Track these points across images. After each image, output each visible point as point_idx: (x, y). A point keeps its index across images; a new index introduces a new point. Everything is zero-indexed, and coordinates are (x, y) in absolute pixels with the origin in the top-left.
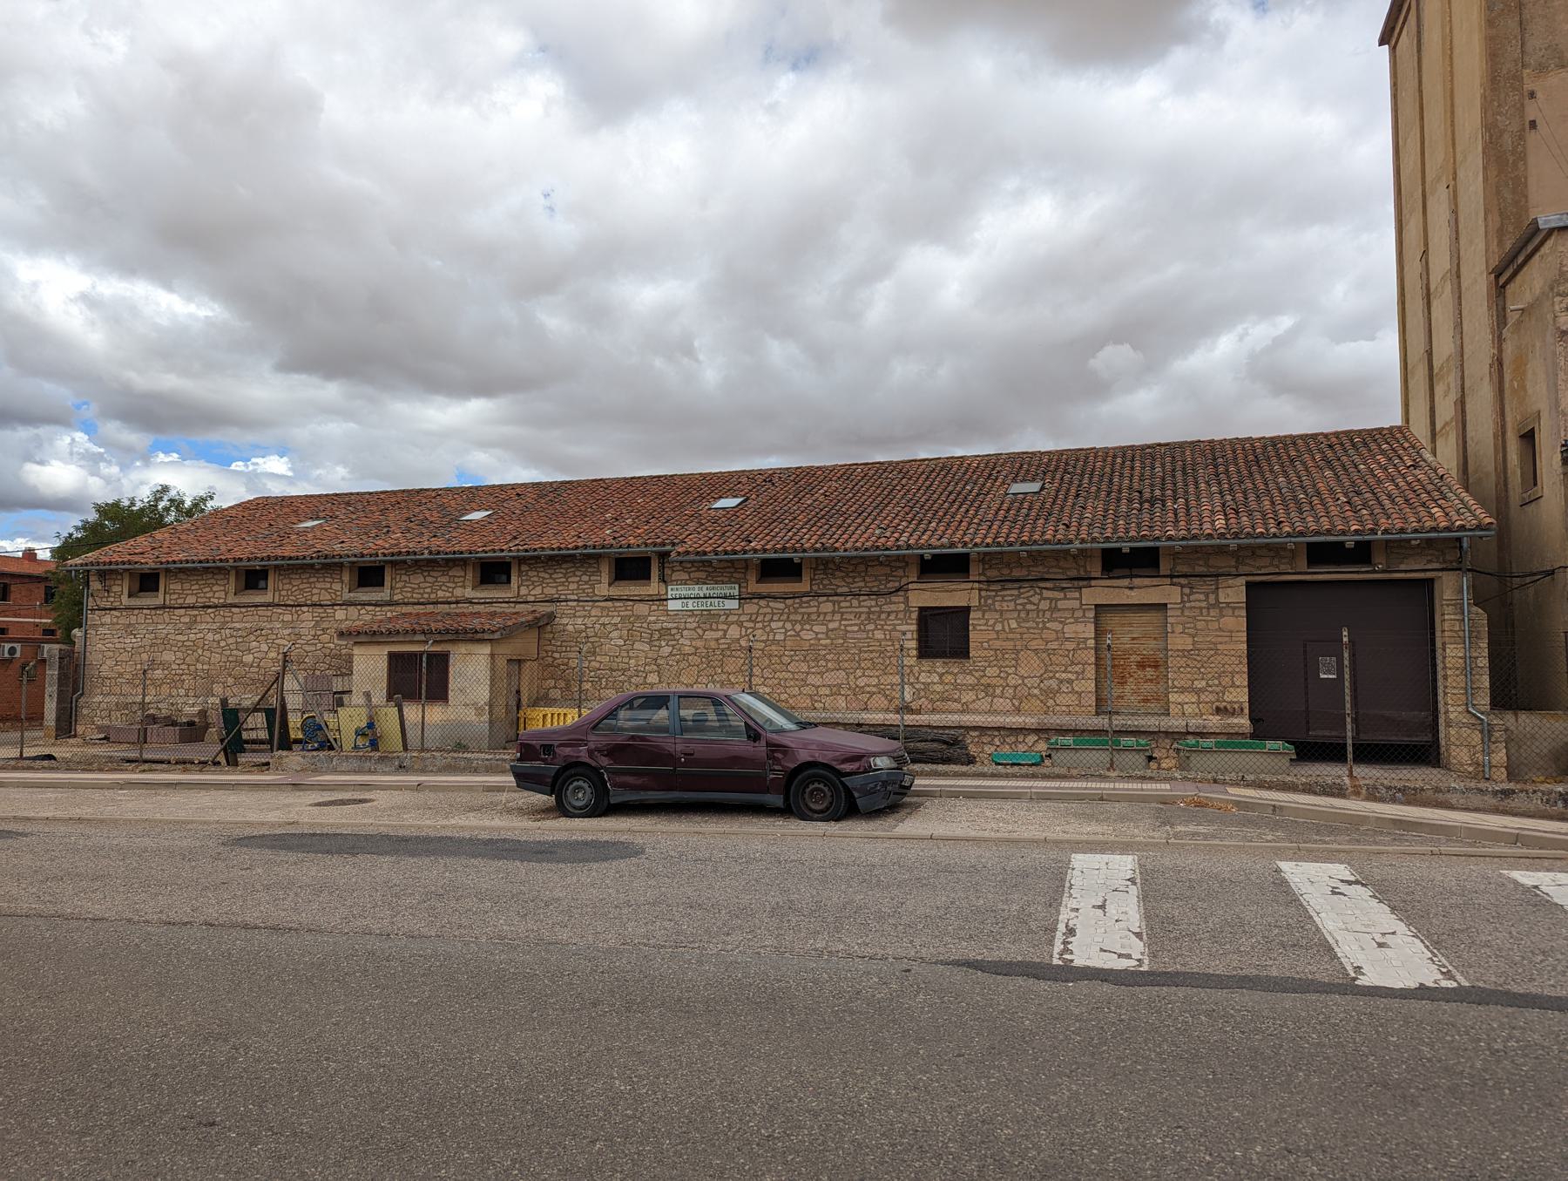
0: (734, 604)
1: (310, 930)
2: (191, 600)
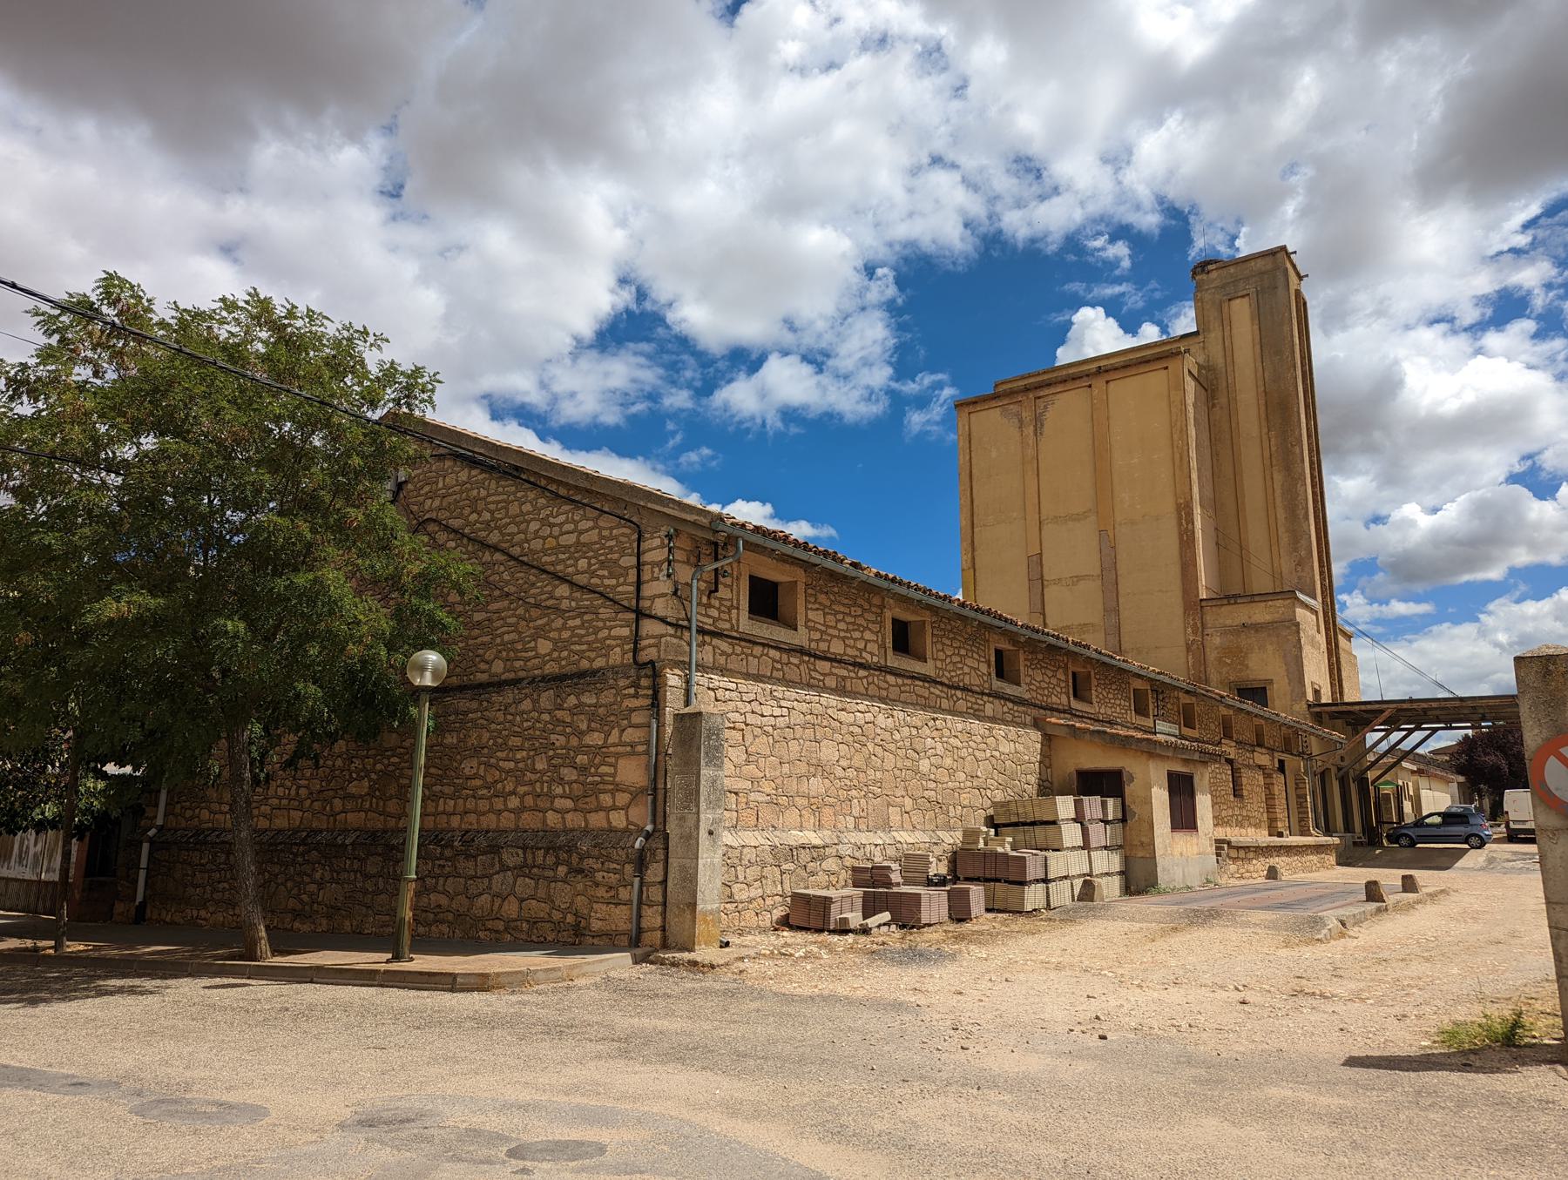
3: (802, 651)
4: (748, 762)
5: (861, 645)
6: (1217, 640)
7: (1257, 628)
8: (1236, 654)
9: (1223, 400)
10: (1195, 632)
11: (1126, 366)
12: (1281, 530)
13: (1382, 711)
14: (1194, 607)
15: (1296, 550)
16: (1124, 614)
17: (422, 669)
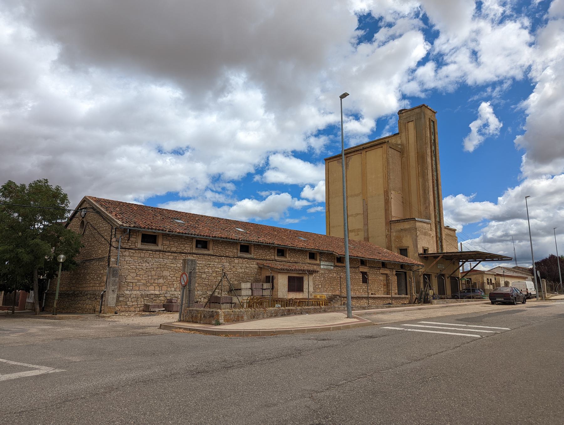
0: (332, 268)
1: (290, 355)
2: (174, 249)
3: (160, 251)
4: (137, 276)
5: (184, 248)
6: (394, 234)
7: (405, 230)
8: (399, 238)
9: (406, 155)
10: (388, 231)
11: (371, 147)
12: (421, 197)
13: (439, 256)
14: (390, 223)
15: (425, 204)
16: (369, 225)
17: (60, 259)
